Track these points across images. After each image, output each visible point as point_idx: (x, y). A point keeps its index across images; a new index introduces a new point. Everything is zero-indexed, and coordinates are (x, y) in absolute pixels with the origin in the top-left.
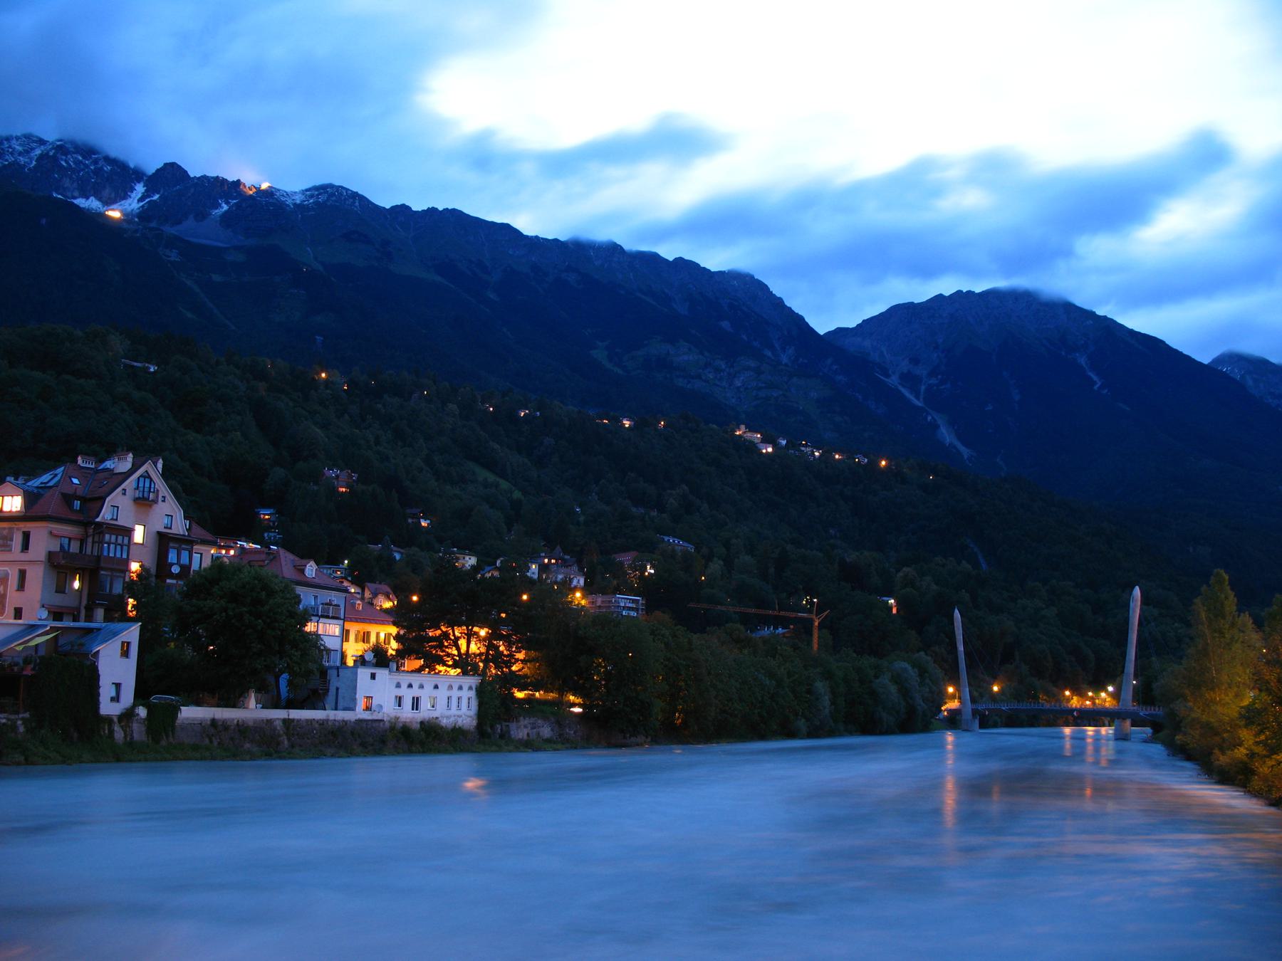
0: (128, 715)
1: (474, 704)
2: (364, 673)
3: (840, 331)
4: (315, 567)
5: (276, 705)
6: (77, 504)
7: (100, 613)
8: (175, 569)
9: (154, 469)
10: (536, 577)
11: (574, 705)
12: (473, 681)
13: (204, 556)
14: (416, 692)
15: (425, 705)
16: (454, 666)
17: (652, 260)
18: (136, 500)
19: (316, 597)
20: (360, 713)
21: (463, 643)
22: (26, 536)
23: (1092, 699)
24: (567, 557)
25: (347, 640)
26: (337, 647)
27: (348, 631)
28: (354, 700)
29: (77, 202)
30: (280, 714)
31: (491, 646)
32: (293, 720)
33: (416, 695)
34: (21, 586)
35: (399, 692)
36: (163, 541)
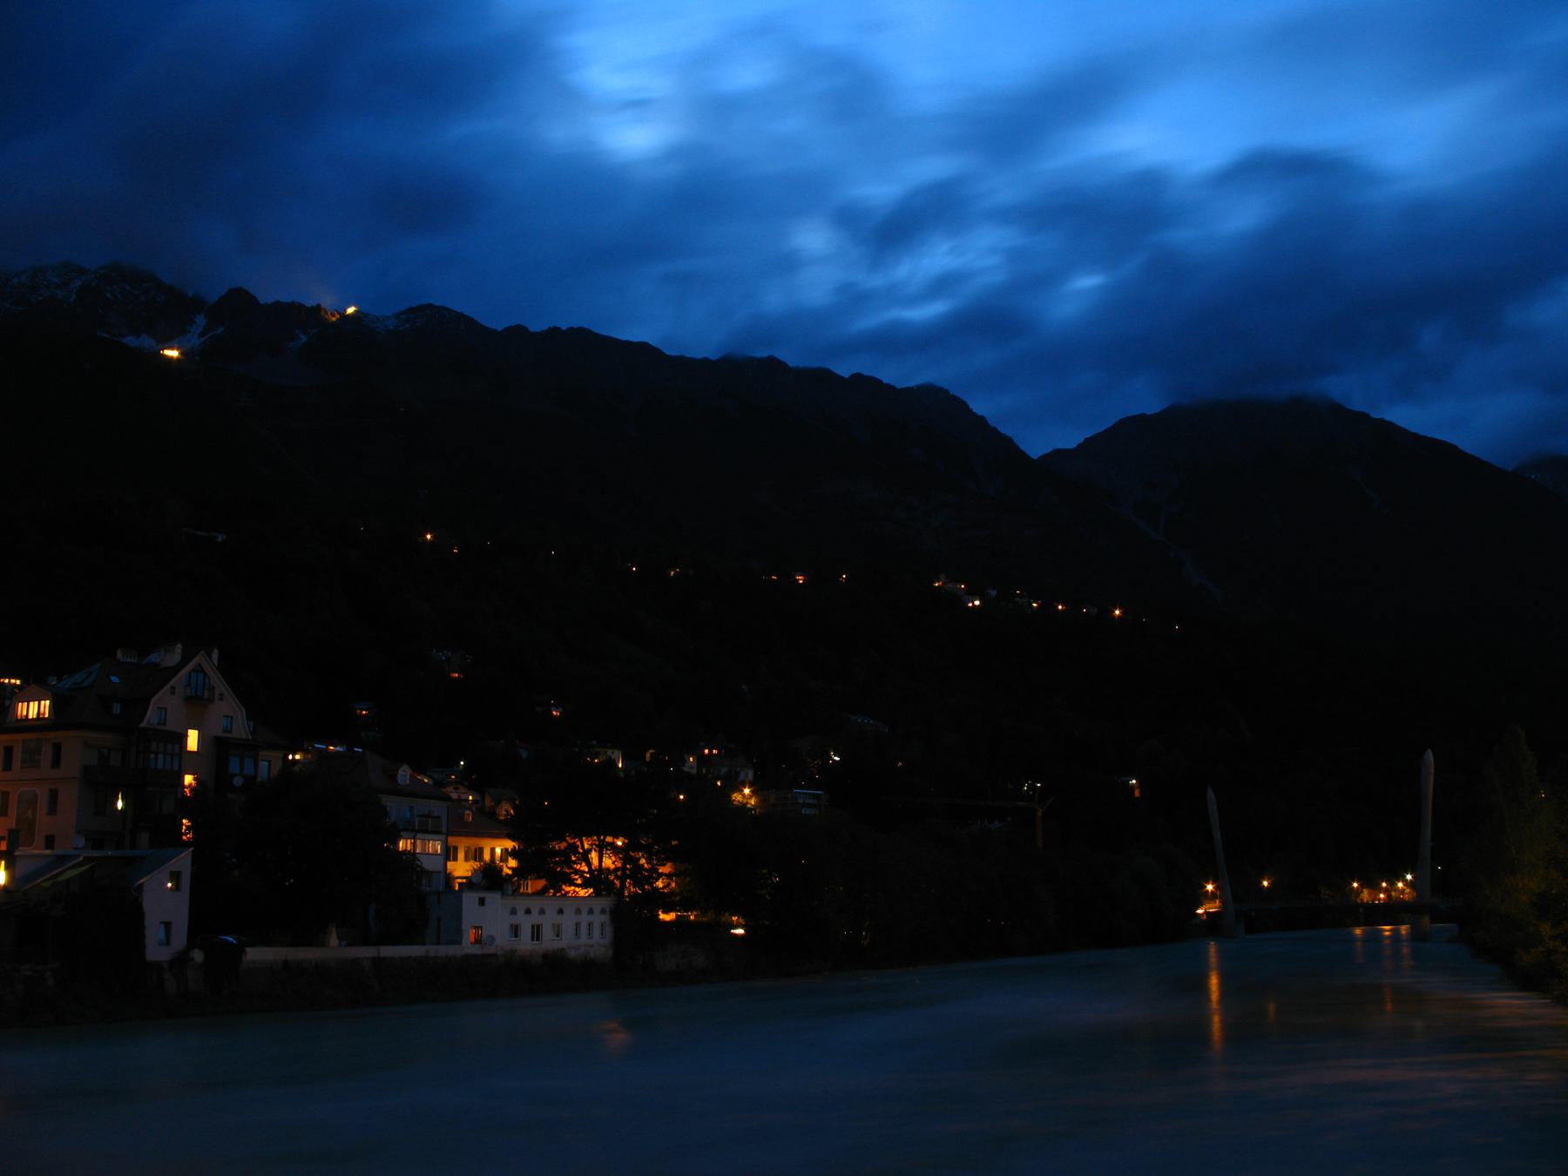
0: (181, 960)
1: (609, 930)
2: (470, 899)
3: (1059, 454)
4: (409, 771)
5: (364, 942)
6: (117, 708)
7: (144, 838)
8: (238, 781)
9: (209, 661)
10: (694, 771)
11: (736, 927)
12: (606, 902)
13: (266, 767)
14: (535, 918)
15: (547, 934)
16: (584, 886)
17: (822, 377)
18: (188, 699)
19: (411, 808)
20: (467, 946)
21: (594, 856)
22: (57, 748)
23: (1386, 891)
25: (455, 859)
26: (440, 868)
27: (456, 849)
28: (459, 931)
29: (125, 341)
30: (368, 952)
32: (384, 959)
33: (536, 922)
34: (53, 808)
35: (516, 920)
36: (215, 746)
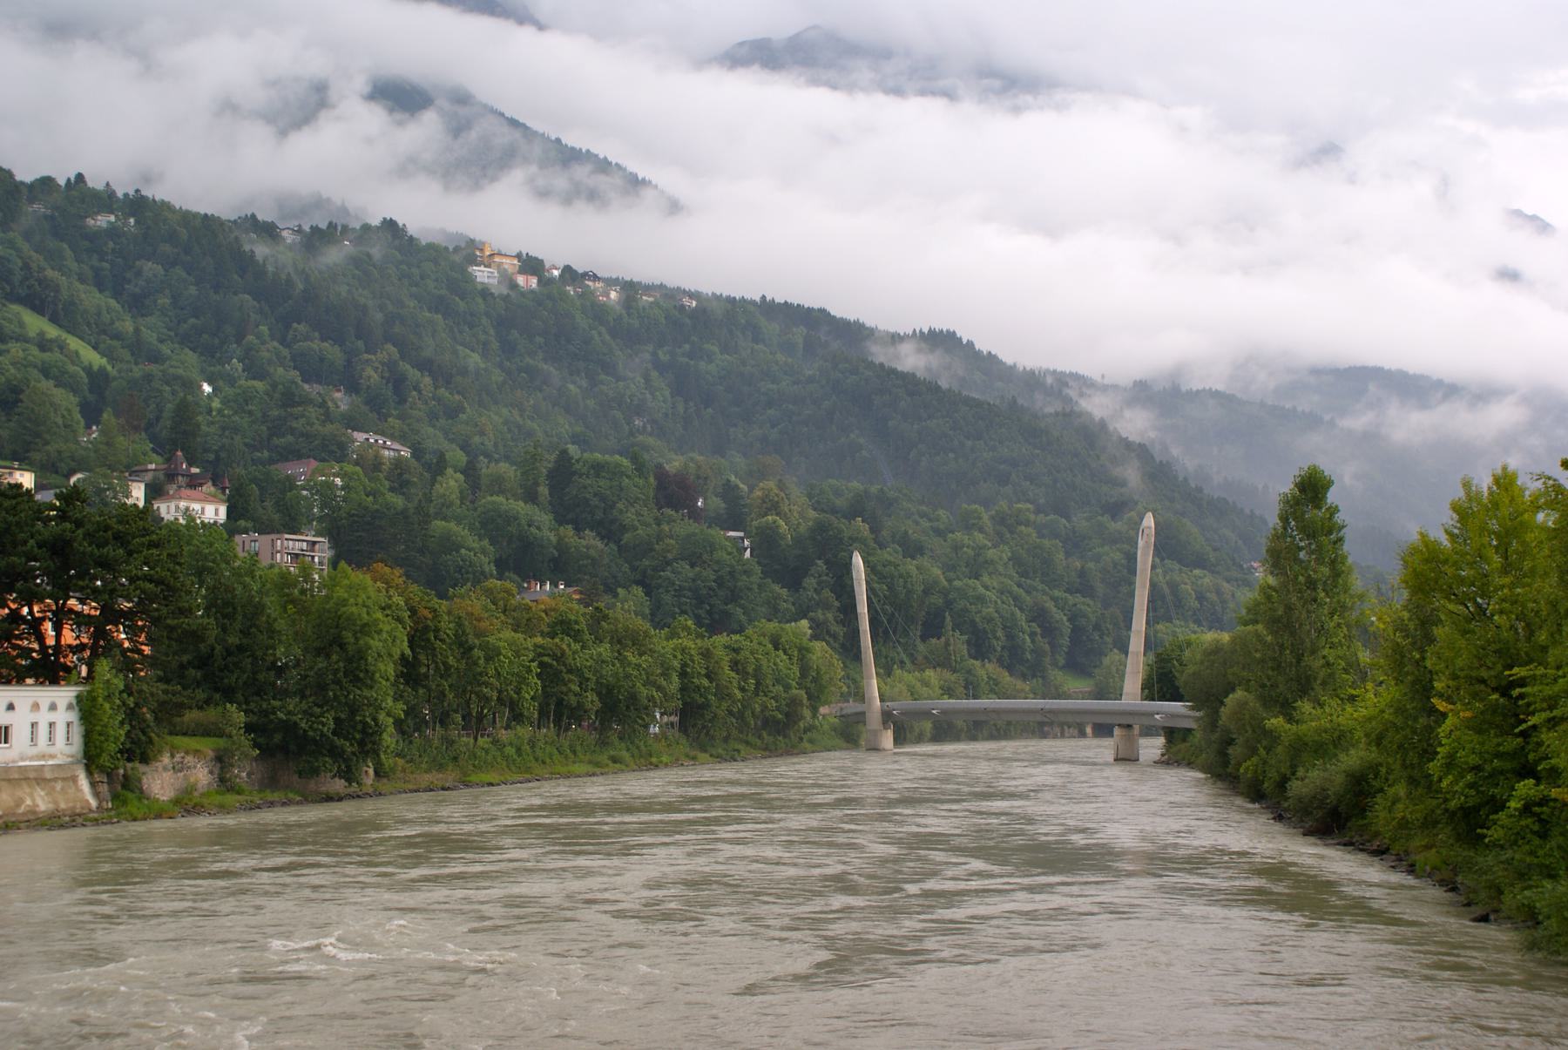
1: (77, 739)
10: (141, 504)
24: (195, 470)
31: (100, 634)
